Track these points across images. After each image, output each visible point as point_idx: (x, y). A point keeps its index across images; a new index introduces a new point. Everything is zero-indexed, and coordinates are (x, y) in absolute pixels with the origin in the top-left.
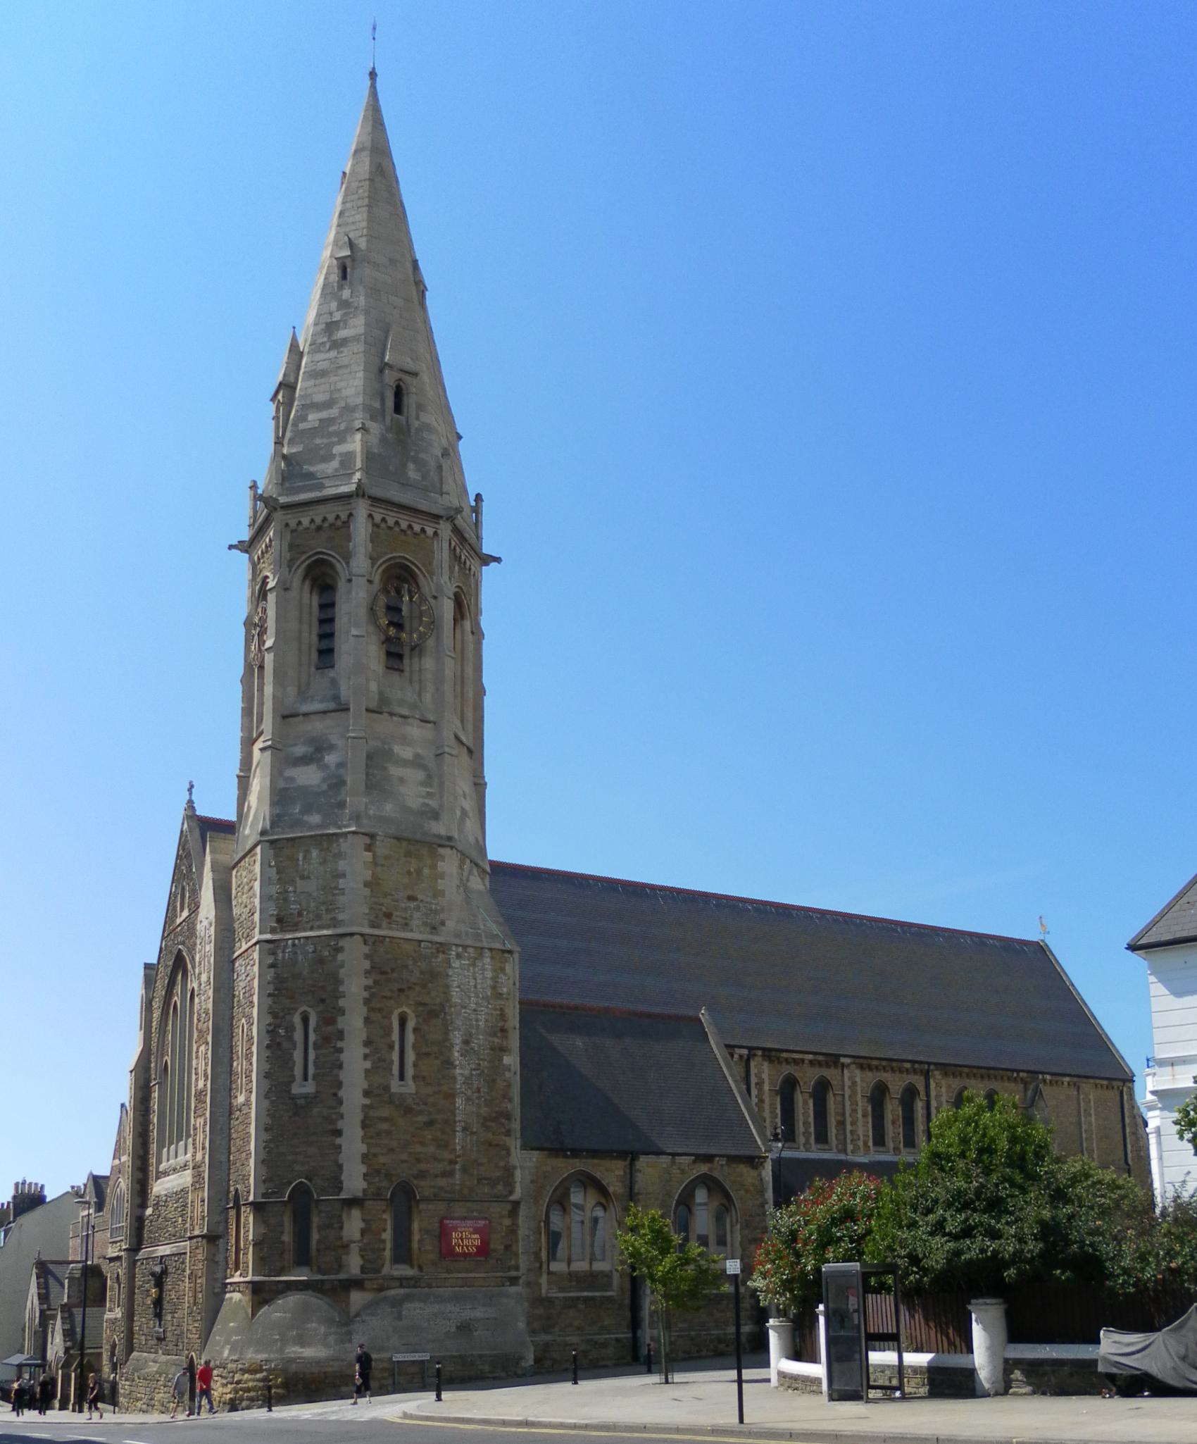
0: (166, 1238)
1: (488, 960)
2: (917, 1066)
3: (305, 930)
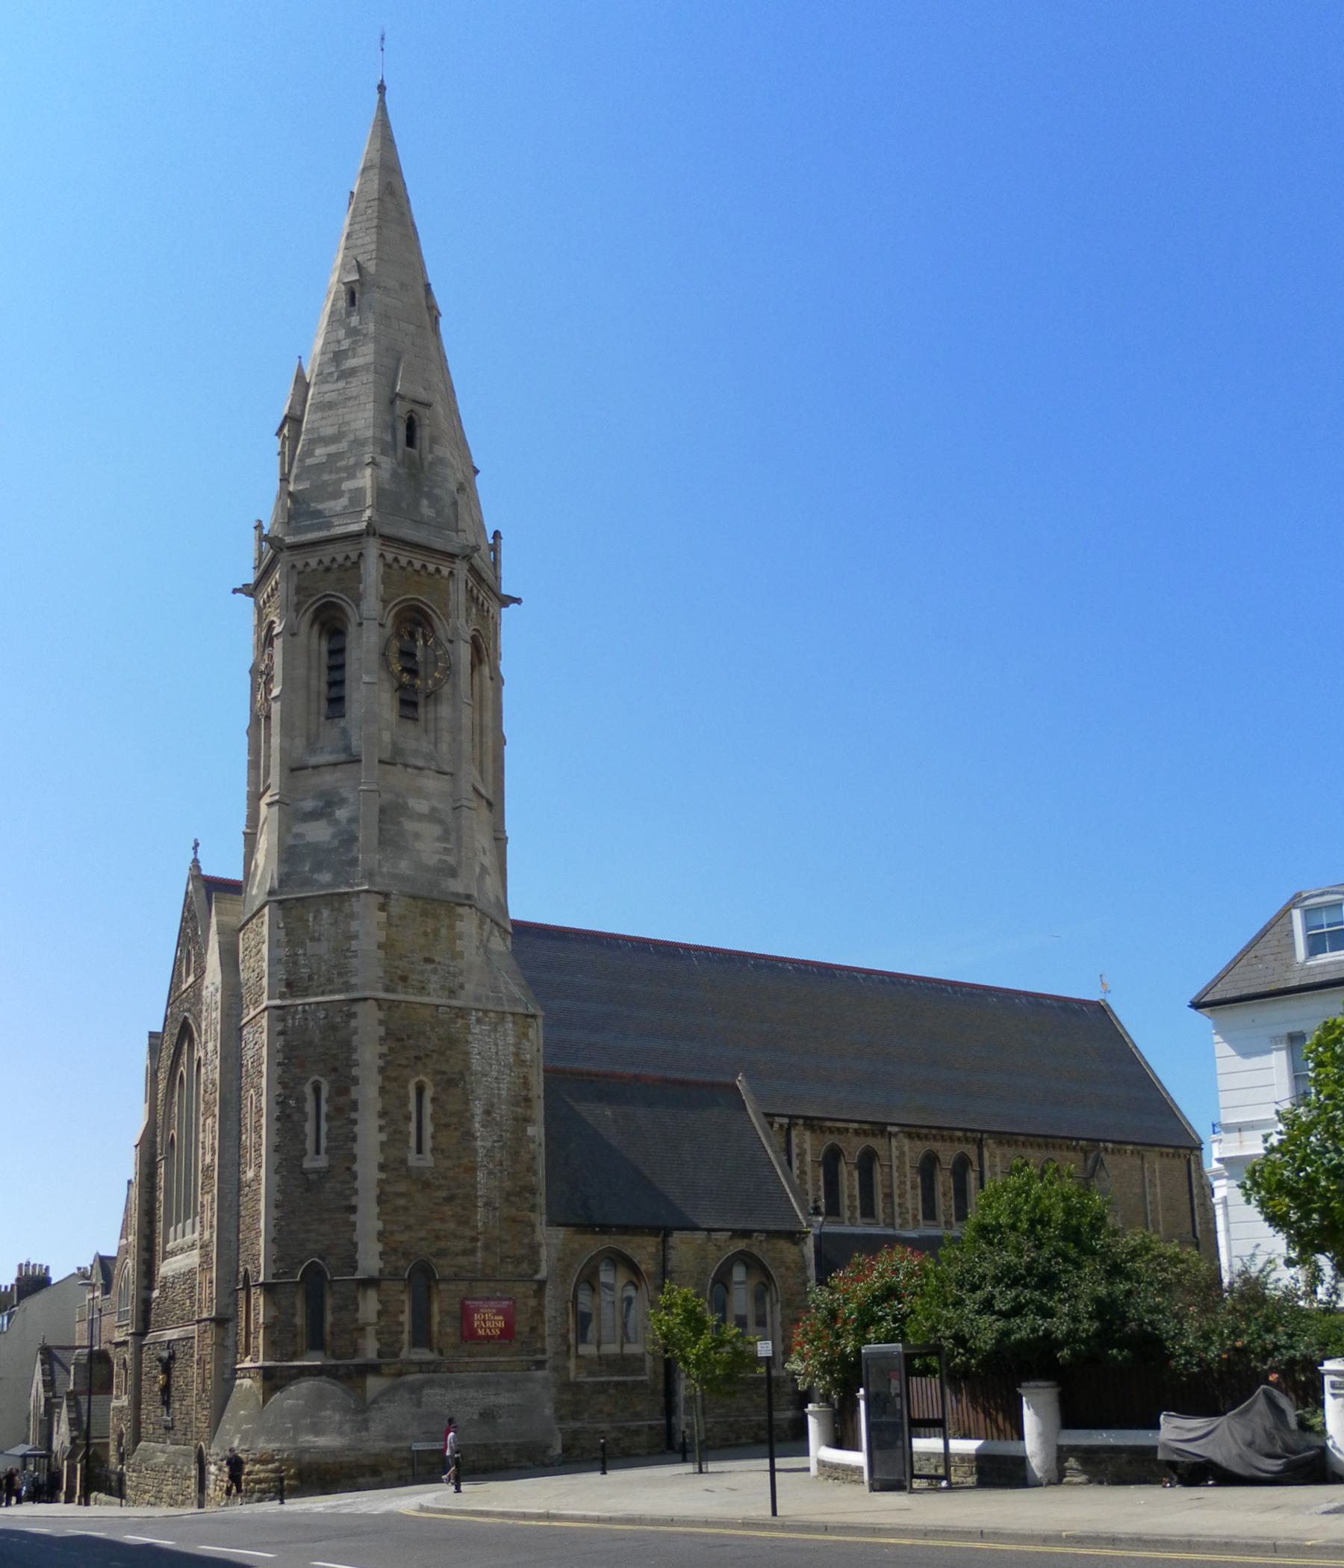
0: (173, 1321)
1: (511, 1025)
2: (969, 1134)
3: (316, 995)
